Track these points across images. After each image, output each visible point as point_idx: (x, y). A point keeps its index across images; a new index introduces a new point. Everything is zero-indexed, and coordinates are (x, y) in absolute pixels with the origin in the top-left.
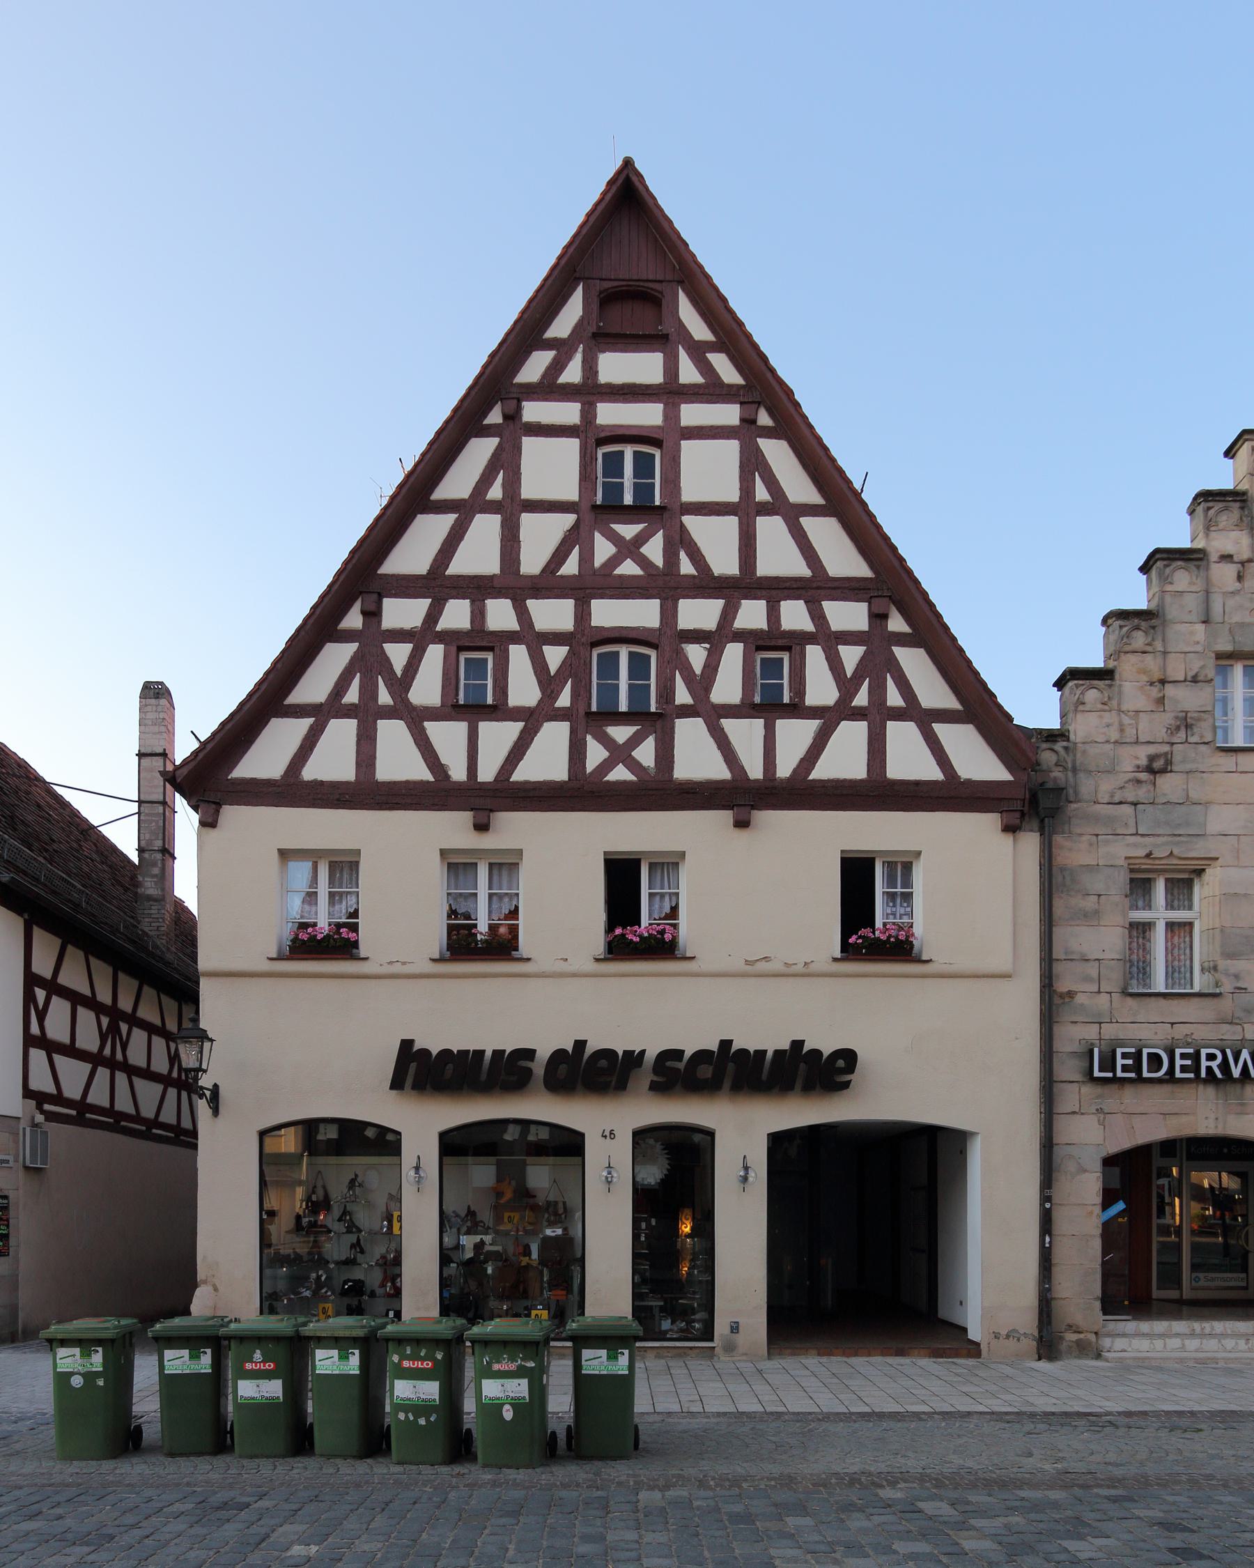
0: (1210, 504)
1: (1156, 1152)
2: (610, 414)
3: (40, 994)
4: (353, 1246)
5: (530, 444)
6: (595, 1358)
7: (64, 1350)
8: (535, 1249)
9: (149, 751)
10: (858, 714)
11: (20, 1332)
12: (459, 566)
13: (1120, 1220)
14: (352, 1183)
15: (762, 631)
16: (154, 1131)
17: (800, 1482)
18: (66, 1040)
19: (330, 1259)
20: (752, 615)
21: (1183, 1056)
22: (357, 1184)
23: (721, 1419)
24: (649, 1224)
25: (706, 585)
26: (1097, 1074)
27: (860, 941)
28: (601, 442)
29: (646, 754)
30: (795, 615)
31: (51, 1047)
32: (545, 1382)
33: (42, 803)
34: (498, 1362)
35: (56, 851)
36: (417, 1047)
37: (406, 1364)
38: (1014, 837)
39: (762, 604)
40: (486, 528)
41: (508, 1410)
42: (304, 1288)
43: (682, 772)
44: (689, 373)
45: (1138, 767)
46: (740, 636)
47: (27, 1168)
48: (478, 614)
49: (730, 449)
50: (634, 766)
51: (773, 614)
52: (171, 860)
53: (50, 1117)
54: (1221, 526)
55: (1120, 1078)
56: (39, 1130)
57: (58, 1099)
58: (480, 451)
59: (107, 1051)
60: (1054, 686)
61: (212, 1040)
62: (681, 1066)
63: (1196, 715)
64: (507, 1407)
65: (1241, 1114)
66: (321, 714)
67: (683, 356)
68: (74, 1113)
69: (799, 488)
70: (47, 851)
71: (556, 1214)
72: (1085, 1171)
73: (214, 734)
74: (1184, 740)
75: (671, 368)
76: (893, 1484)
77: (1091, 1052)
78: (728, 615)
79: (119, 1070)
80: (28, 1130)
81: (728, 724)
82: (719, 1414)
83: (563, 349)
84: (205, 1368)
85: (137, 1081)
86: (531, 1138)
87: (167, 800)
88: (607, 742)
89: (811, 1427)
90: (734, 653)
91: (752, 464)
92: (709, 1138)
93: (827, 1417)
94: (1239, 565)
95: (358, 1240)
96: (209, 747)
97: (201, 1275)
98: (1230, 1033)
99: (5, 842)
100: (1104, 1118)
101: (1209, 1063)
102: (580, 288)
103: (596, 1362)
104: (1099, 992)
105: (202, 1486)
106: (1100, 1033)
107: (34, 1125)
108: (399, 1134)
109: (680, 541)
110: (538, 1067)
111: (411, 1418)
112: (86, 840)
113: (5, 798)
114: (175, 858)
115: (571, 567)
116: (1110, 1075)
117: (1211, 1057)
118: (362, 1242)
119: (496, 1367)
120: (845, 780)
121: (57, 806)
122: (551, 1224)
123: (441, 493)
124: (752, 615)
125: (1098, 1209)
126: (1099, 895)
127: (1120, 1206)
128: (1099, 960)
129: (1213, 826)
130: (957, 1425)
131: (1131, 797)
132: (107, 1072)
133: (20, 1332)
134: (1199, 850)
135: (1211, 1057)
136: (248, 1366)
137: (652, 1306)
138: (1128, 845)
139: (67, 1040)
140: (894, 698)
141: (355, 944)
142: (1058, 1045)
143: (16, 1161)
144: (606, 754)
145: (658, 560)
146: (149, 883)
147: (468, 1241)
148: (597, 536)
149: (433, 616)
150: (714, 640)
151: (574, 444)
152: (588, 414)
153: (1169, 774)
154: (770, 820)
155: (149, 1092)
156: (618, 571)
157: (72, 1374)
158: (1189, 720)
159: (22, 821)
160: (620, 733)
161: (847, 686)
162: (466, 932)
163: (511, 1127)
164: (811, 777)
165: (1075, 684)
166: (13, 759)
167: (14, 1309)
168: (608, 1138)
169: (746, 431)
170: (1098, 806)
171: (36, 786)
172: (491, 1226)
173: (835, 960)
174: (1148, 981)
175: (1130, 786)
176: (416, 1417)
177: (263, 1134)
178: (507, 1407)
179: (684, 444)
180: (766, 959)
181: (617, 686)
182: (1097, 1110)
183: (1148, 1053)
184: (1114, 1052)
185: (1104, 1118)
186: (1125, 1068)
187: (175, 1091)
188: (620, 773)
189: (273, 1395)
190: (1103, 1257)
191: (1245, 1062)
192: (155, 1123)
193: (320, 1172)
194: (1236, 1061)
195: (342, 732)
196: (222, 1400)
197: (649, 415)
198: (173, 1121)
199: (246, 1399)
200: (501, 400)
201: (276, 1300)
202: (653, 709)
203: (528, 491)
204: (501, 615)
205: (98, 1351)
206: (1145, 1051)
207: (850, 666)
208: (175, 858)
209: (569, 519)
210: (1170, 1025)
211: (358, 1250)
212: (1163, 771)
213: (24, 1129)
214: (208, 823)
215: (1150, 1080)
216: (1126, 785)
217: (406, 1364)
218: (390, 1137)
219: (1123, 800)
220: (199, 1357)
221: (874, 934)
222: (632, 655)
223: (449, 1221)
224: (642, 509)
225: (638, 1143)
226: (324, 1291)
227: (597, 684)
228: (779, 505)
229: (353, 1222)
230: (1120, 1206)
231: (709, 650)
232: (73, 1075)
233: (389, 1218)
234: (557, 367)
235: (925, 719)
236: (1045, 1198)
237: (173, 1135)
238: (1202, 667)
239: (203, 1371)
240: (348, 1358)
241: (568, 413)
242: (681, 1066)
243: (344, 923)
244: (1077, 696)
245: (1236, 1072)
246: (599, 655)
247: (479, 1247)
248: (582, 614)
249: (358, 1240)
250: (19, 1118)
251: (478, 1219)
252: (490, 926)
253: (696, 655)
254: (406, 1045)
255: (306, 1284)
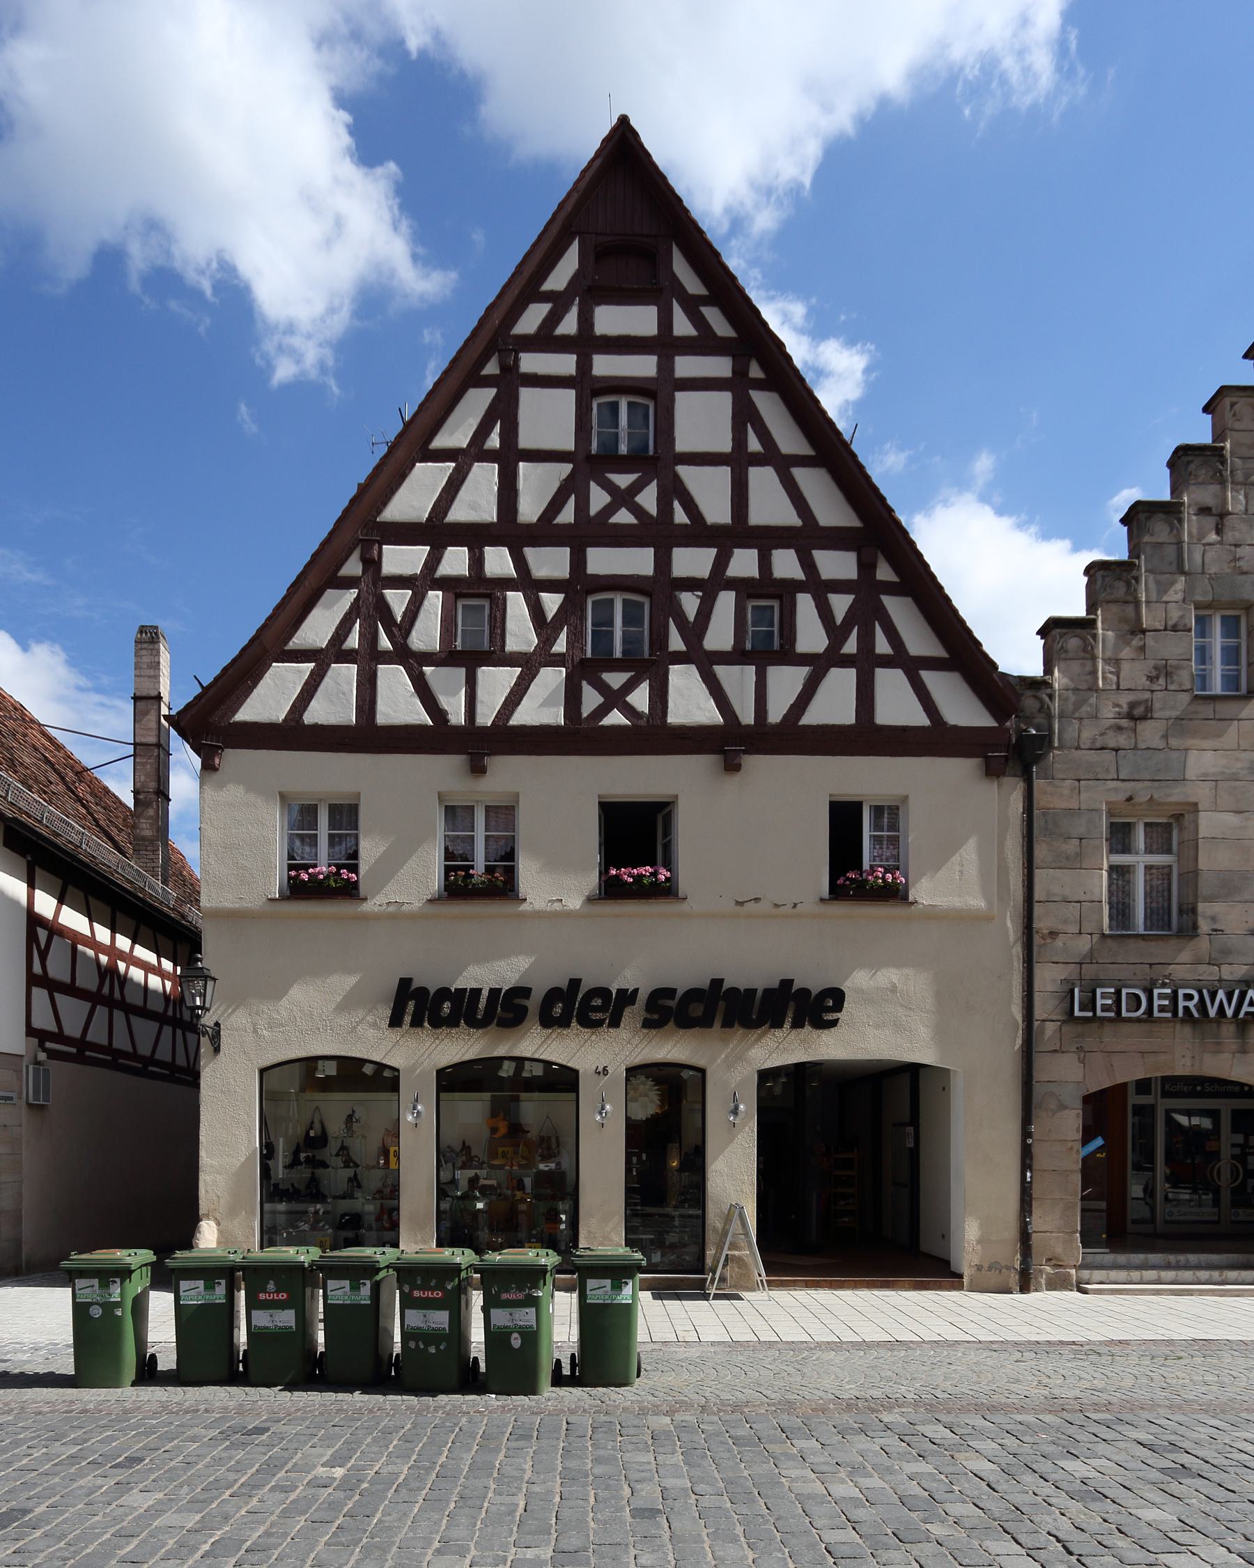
0: (1190, 458)
1: (1131, 1090)
2: (604, 365)
3: (42, 934)
4: (350, 1180)
5: (527, 396)
6: (599, 1288)
7: (83, 1281)
8: (528, 1181)
9: (144, 693)
10: (846, 662)
11: (24, 1266)
12: (459, 513)
13: (1098, 1155)
14: (350, 1118)
15: (752, 579)
16: (150, 1068)
17: (800, 1408)
18: (67, 979)
19: (326, 1193)
20: (744, 563)
21: (1161, 996)
22: (354, 1120)
23: (718, 1349)
24: (639, 1158)
25: (699, 533)
26: (1077, 1013)
27: (848, 883)
28: (597, 393)
29: (640, 698)
30: (786, 564)
31: (53, 987)
32: (551, 1311)
33: (38, 745)
34: (507, 1291)
35: (54, 793)
36: (415, 985)
37: (416, 1294)
38: (998, 781)
39: (754, 553)
40: (484, 477)
41: (516, 1338)
42: (302, 1222)
43: (676, 716)
44: (682, 326)
45: (1119, 714)
46: (734, 584)
47: (29, 1105)
48: (477, 562)
49: (724, 400)
50: (629, 711)
51: (765, 563)
52: (166, 802)
53: (52, 1055)
54: (1200, 479)
55: (1100, 1017)
56: (41, 1068)
57: (59, 1037)
58: (478, 400)
59: (106, 990)
60: (1038, 633)
61: (214, 979)
62: (672, 1003)
63: (1175, 663)
64: (515, 1335)
65: (1216, 1052)
66: (322, 659)
67: (677, 311)
68: (74, 1050)
69: (789, 440)
70: (45, 792)
71: (549, 1148)
72: (1065, 1108)
73: (217, 679)
74: (1164, 688)
75: (665, 321)
76: (889, 1409)
77: (1072, 992)
78: (721, 563)
79: (117, 1009)
80: (31, 1067)
81: (721, 671)
82: (713, 1343)
83: (560, 302)
84: (220, 1299)
85: (135, 1020)
86: (525, 1074)
87: (162, 742)
88: (602, 688)
89: (804, 1355)
90: (726, 602)
91: (745, 416)
92: (700, 1075)
93: (819, 1345)
94: (1217, 518)
95: (356, 1175)
96: (212, 691)
97: (203, 1210)
98: (1208, 973)
99: (9, 785)
100: (1085, 1056)
101: (1187, 1004)
102: (575, 245)
103: (600, 1292)
104: (1080, 933)
105: (220, 1413)
106: (1080, 973)
107: (37, 1063)
108: (398, 1070)
109: (674, 491)
110: (534, 1003)
111: (422, 1346)
112: (81, 781)
113: (4, 740)
114: (170, 800)
115: (567, 515)
116: (1090, 1014)
117: (1189, 997)
118: (359, 1177)
119: (505, 1296)
120: (833, 726)
121: (52, 748)
122: (544, 1158)
123: (441, 441)
124: (744, 563)
125: (1078, 1145)
126: (1081, 839)
127: (1099, 1142)
128: (1080, 902)
129: (1191, 773)
130: (946, 1353)
131: (1112, 744)
132: (105, 1010)
133: (24, 1266)
134: (1176, 795)
135: (1189, 997)
136: (262, 1296)
137: (642, 1239)
138: (1109, 790)
139: (68, 980)
140: (882, 646)
141: (355, 885)
142: (1037, 985)
143: (20, 1098)
144: (601, 700)
145: (652, 508)
146: (144, 825)
147: (463, 1176)
148: (593, 485)
149: (433, 561)
150: (709, 588)
151: (570, 395)
152: (584, 365)
153: (1149, 721)
154: (758, 765)
155: (145, 1030)
156: (613, 520)
157: (91, 1304)
158: (1168, 668)
159: (21, 763)
160: (616, 680)
161: (836, 633)
162: (463, 873)
163: (506, 1064)
164: (801, 723)
165: (1059, 633)
166: (10, 702)
167: (18, 1243)
168: (602, 1074)
169: (738, 385)
170: (1079, 752)
171: (32, 728)
172: (486, 1160)
173: (822, 900)
174: (1127, 923)
175: (1111, 733)
176: (427, 1345)
177: (262, 1071)
178: (515, 1335)
179: (679, 395)
180: (757, 900)
181: (612, 632)
182: (1077, 1048)
183: (1127, 993)
184: (1094, 992)
185: (1085, 1056)
186: (1105, 1008)
187: (171, 1028)
188: (616, 718)
189: (285, 1325)
190: (1082, 1192)
191: (1221, 1001)
192: (151, 1060)
193: (317, 1108)
194: (1213, 1002)
195: (345, 675)
196: (236, 1330)
197: (644, 366)
198: (168, 1059)
199: (259, 1328)
200: (499, 351)
201: (275, 1233)
202: (646, 656)
203: (525, 441)
204: (498, 561)
205: (116, 1282)
206: (1124, 991)
207: (839, 616)
208: (170, 800)
209: (566, 469)
210: (1148, 966)
211: (355, 1184)
212: (1144, 718)
213: (27, 1067)
214: (208, 767)
215: (1130, 1020)
216: (1108, 731)
217: (416, 1294)
218: (387, 1074)
219: (1105, 746)
220: (213, 1288)
221: (861, 875)
222: (626, 603)
223: (444, 1156)
224: (637, 461)
225: (629, 1080)
226: (321, 1224)
227: (592, 630)
228: (771, 456)
229: (350, 1157)
230: (1099, 1142)
231: (702, 598)
232: (73, 1014)
233: (385, 1152)
234: (554, 319)
235: (912, 667)
236: (1026, 1134)
237: (168, 1072)
238: (1182, 617)
239: (217, 1301)
240: (359, 1288)
241: (565, 364)
242: (672, 1003)
243: (344, 864)
244: (1060, 644)
245: (1212, 1012)
246: (593, 603)
247: (473, 1181)
248: (578, 562)
249: (356, 1175)
250: (22, 1056)
251: (473, 1154)
252: (487, 867)
253: (690, 603)
254: (405, 983)
255: (304, 1219)
